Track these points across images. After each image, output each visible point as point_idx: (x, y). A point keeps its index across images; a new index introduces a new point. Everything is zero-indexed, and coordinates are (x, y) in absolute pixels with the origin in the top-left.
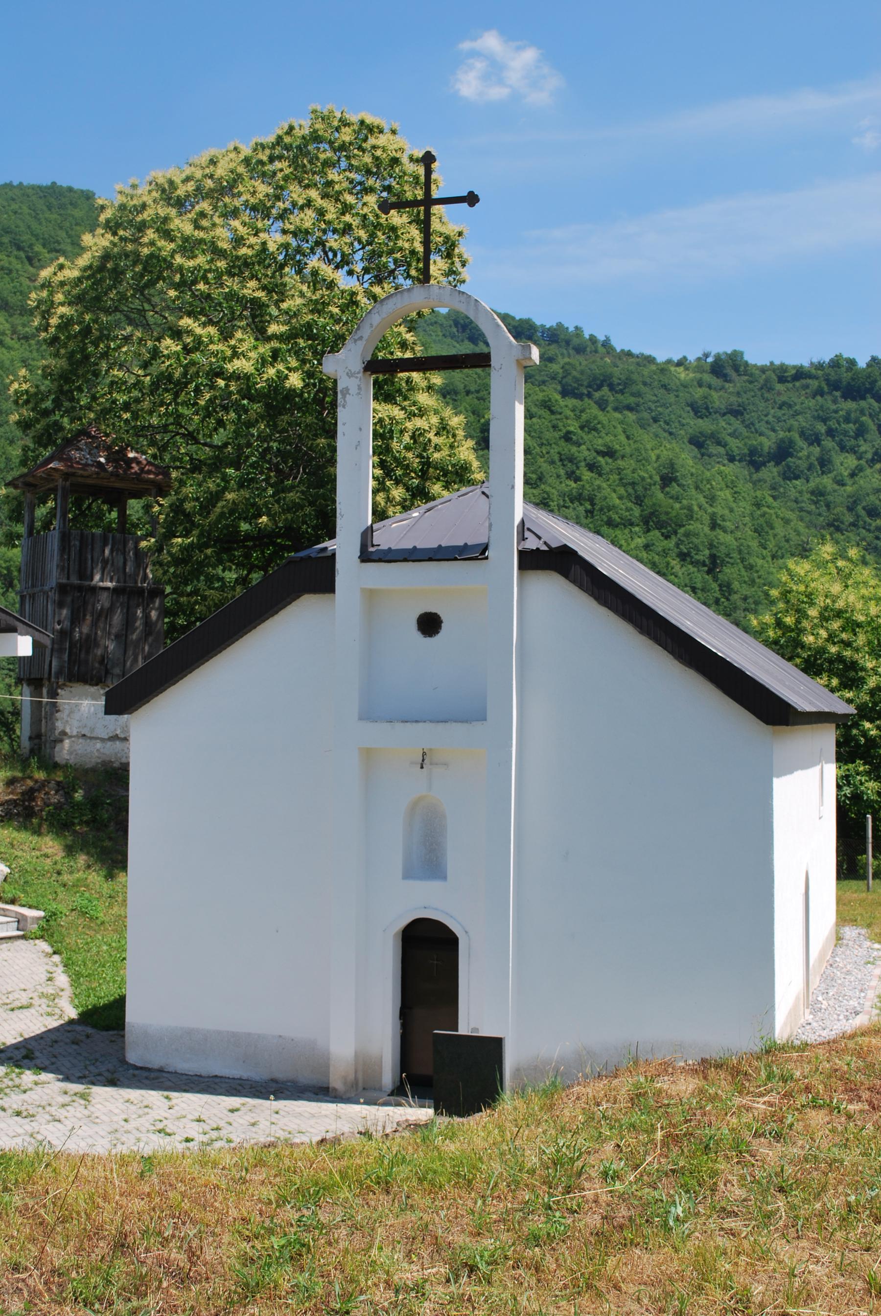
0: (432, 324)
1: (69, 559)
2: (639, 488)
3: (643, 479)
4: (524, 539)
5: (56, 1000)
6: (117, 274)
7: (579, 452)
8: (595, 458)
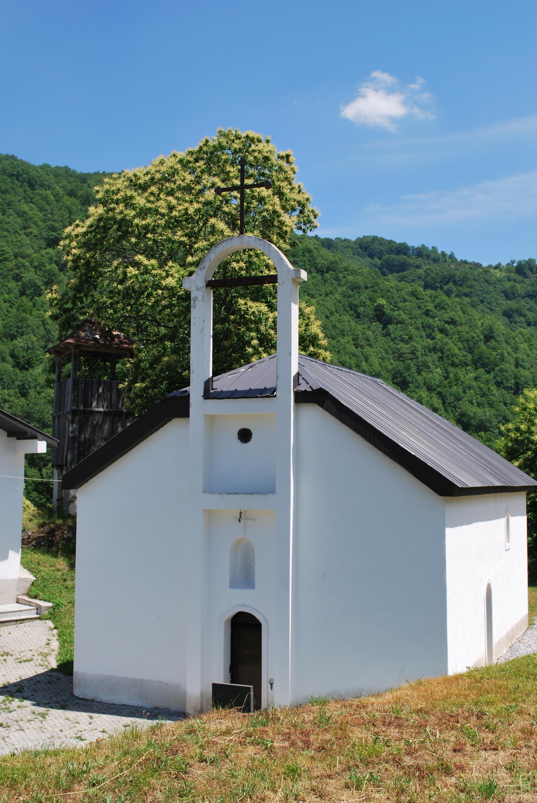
0: (346, 247)
1: (78, 394)
2: (471, 343)
3: (473, 337)
4: (299, 384)
5: (48, 657)
6: (106, 229)
7: (434, 322)
8: (444, 326)
